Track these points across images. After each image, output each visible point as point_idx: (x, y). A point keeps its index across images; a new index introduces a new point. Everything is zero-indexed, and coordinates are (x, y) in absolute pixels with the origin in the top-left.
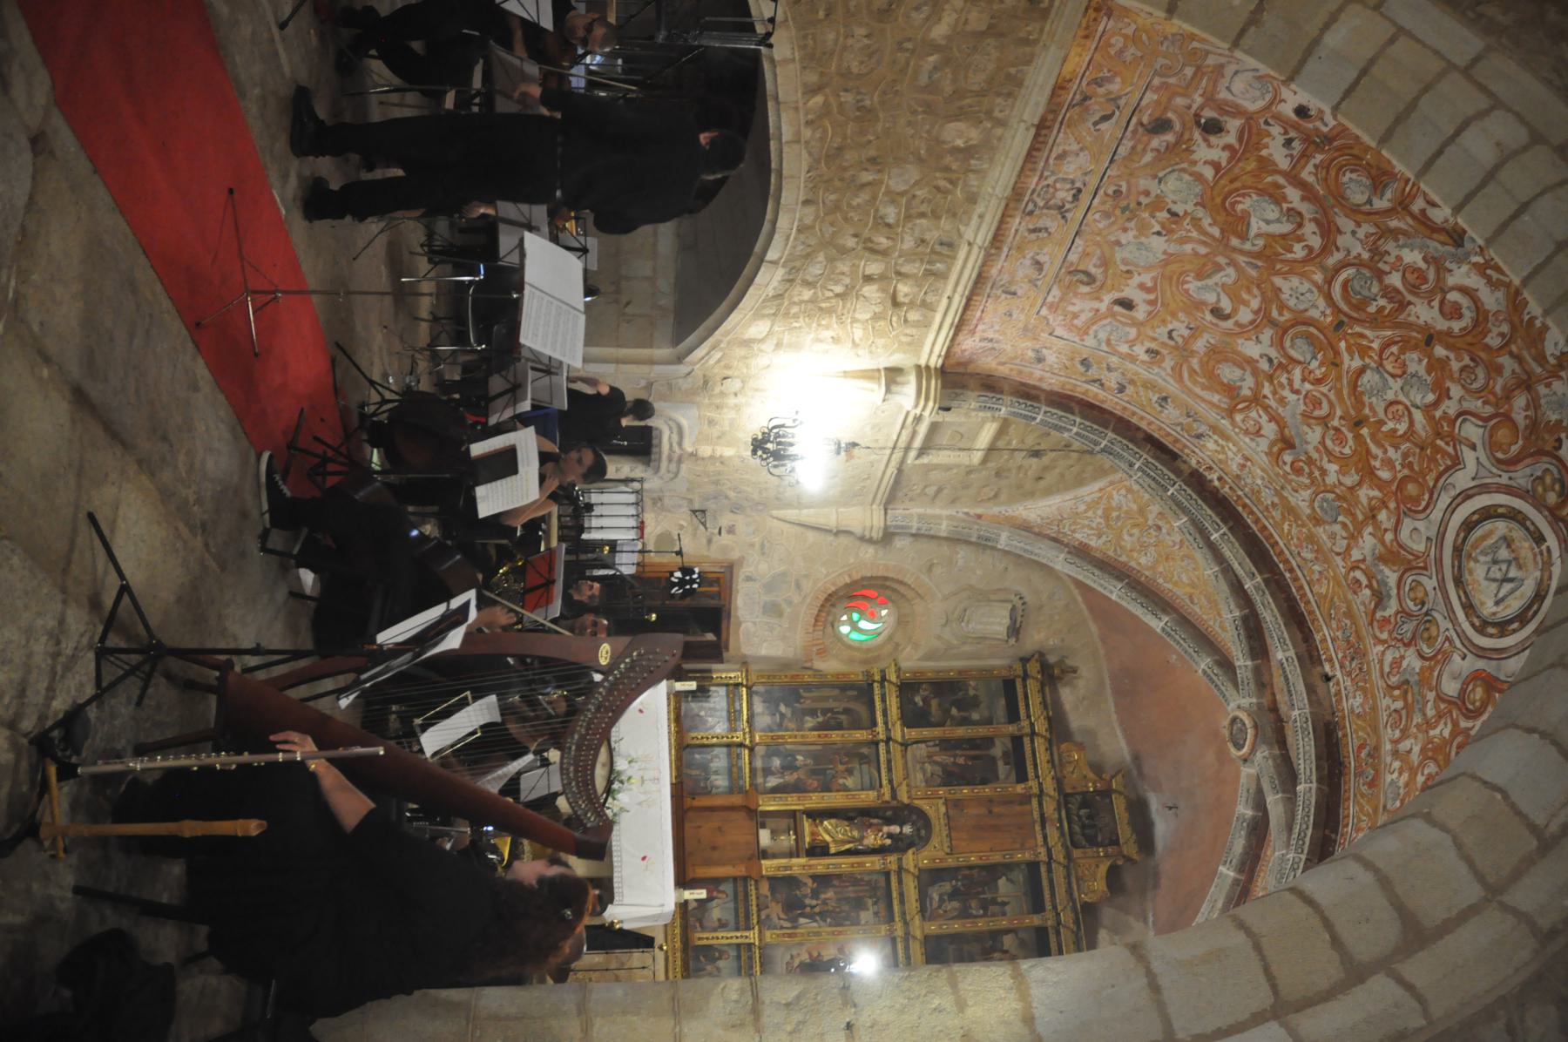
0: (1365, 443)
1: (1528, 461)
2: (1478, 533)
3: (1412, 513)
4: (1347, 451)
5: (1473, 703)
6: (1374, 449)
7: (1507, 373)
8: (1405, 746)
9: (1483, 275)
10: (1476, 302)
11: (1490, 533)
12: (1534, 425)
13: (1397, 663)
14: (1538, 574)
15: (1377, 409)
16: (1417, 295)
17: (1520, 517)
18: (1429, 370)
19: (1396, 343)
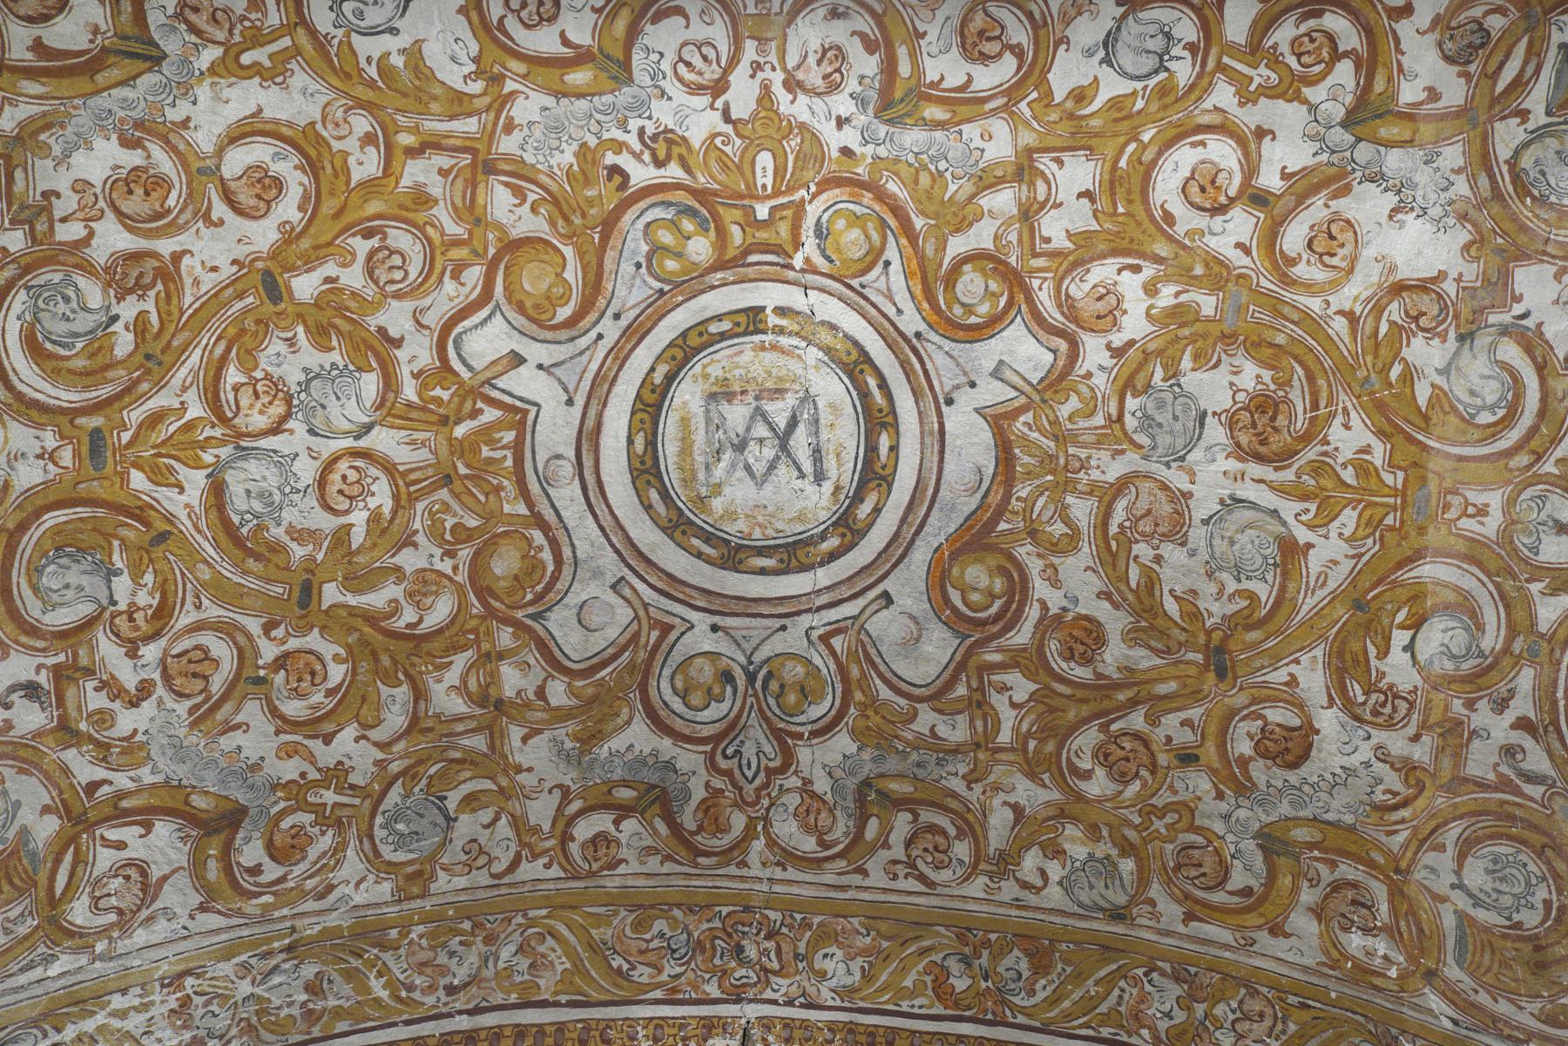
0: (353, 611)
1: (610, 255)
2: (670, 450)
3: (545, 600)
4: (337, 673)
5: (993, 597)
6: (376, 600)
7: (436, 187)
8: (999, 821)
10: (272, 131)
11: (685, 422)
12: (557, 205)
14: (813, 354)
15: (310, 524)
16: (174, 229)
17: (694, 340)
18: (321, 335)
19: (223, 361)
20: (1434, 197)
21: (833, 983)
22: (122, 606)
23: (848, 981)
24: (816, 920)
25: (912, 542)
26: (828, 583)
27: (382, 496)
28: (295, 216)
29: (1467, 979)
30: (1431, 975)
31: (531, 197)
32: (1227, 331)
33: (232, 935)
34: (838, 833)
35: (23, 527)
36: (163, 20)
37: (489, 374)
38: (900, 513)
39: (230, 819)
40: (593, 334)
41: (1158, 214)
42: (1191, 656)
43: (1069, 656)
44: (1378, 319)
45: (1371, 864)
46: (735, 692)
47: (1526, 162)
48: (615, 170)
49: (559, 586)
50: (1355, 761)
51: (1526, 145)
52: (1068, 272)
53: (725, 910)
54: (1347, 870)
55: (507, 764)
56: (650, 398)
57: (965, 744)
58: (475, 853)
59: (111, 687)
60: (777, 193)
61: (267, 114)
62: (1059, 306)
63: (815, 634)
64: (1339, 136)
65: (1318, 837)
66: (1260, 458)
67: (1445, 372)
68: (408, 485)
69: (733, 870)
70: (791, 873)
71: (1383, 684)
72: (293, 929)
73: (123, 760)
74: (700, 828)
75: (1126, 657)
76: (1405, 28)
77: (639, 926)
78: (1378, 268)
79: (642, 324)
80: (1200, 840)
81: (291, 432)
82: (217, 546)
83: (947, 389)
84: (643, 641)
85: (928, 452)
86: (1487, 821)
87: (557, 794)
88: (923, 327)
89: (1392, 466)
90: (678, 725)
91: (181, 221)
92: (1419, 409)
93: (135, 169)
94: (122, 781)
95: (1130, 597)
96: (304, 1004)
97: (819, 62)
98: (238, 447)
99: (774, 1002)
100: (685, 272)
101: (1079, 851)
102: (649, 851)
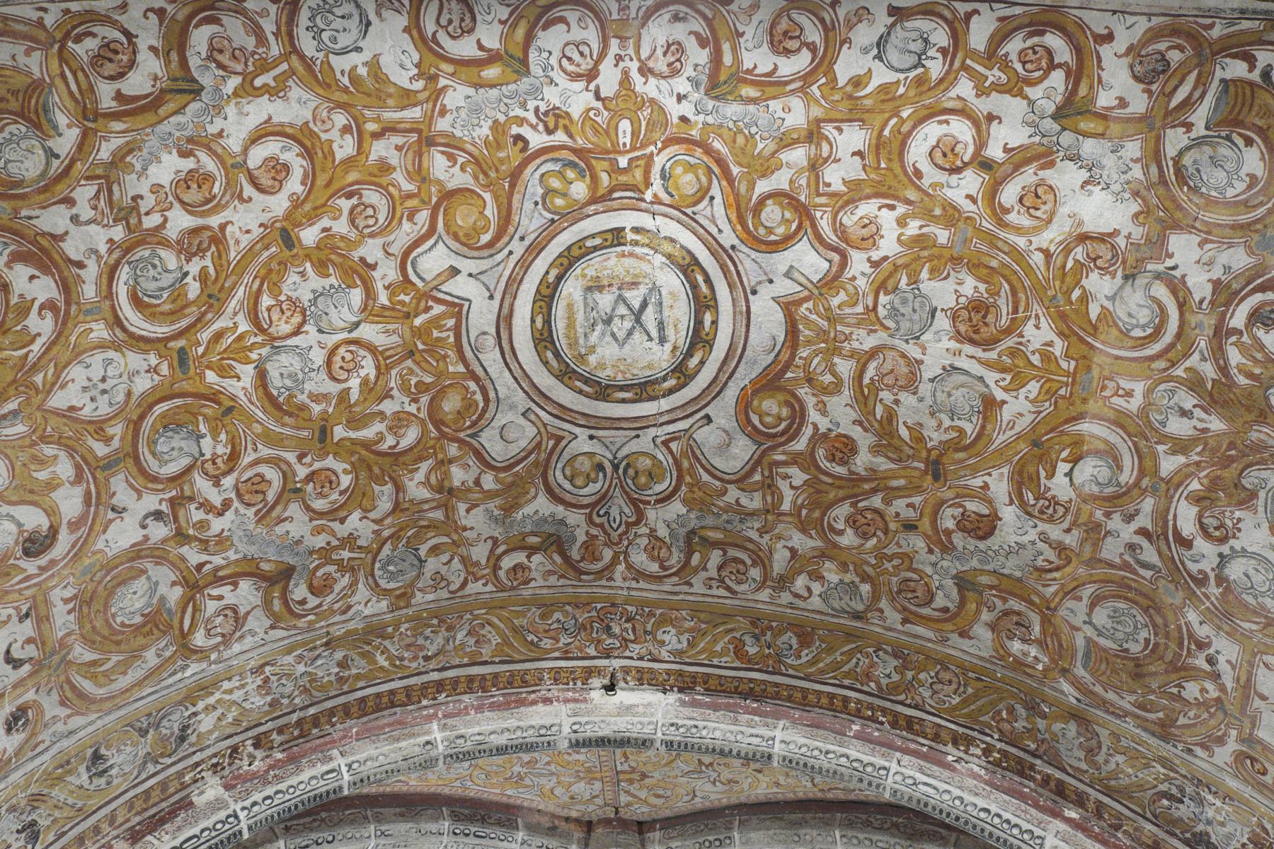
0: (354, 442)
2: (560, 325)
4: (346, 481)
5: (780, 419)
6: (368, 433)
8: (780, 559)
9: (258, 92)
11: (570, 306)
12: (479, 165)
13: (655, 545)
15: (322, 390)
17: (575, 252)
18: (322, 267)
19: (259, 291)
20: (1115, 177)
21: (669, 648)
22: (208, 456)
23: (679, 647)
24: (658, 612)
25: (726, 383)
26: (668, 408)
27: (368, 368)
28: (299, 189)
29: (1088, 676)
30: (1064, 671)
31: (460, 160)
32: (955, 255)
33: (291, 640)
34: (674, 561)
35: (142, 417)
36: (200, 62)
37: (435, 283)
38: (718, 365)
39: (286, 573)
40: (506, 251)
41: (910, 170)
42: (916, 464)
43: (832, 459)
44: (1066, 257)
45: (1031, 603)
46: (605, 476)
47: (1187, 160)
48: (519, 138)
49: (487, 415)
50: (1025, 539)
51: (1188, 148)
52: (842, 207)
53: (599, 606)
54: (1014, 604)
55: (457, 526)
56: (546, 292)
57: (759, 510)
58: (439, 580)
59: (206, 506)
60: (633, 149)
61: (275, 120)
62: (835, 231)
63: (659, 440)
64: (1049, 125)
65: (996, 582)
66: (973, 342)
67: (1112, 298)
68: (385, 359)
69: (604, 582)
70: (642, 584)
71: (1048, 495)
72: (328, 633)
73: (217, 548)
74: (583, 559)
75: (872, 462)
76: (1106, 51)
77: (543, 616)
78: (1069, 222)
79: (539, 243)
80: (915, 576)
81: (307, 333)
82: (265, 411)
83: (753, 284)
84: (543, 447)
85: (738, 325)
86: (1112, 587)
87: (490, 542)
88: (736, 242)
89: (1067, 356)
90: (568, 497)
91: (223, 202)
92: (1090, 322)
93: (190, 171)
94: (218, 560)
95: (876, 424)
96: (337, 674)
97: (665, 54)
98: (273, 347)
99: (631, 658)
100: (568, 206)
101: (833, 578)
102: (550, 573)
